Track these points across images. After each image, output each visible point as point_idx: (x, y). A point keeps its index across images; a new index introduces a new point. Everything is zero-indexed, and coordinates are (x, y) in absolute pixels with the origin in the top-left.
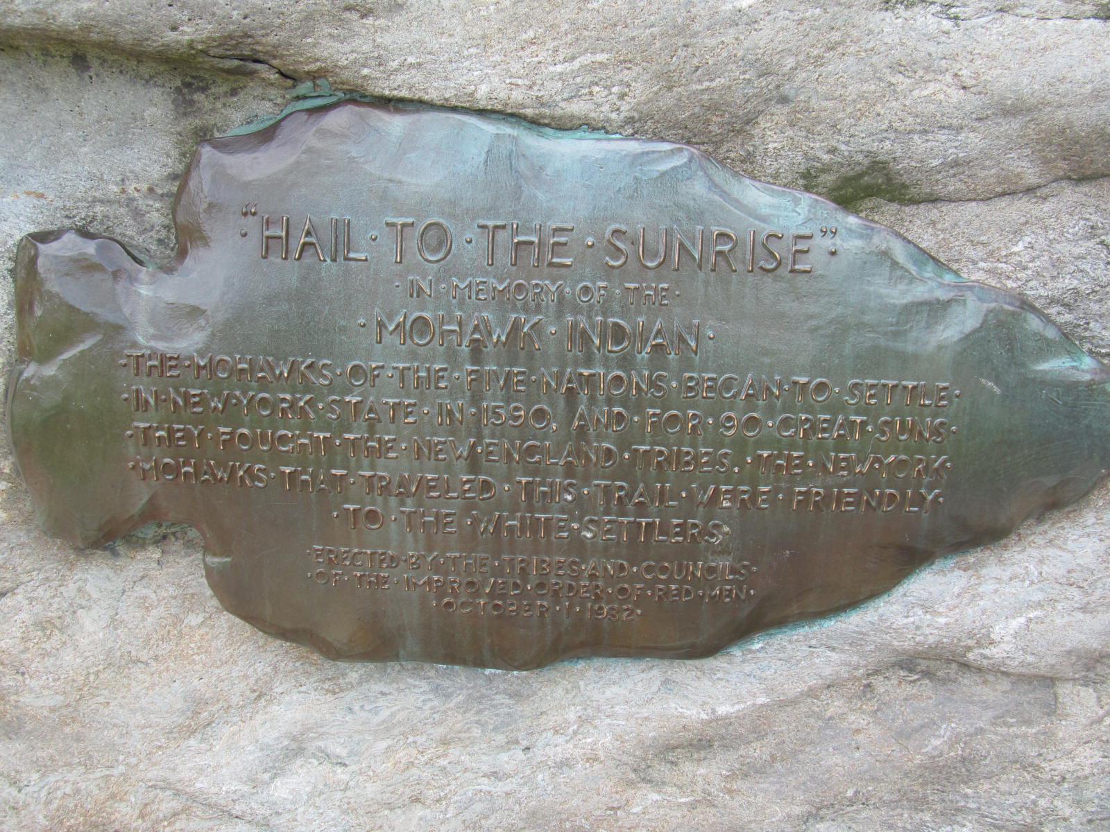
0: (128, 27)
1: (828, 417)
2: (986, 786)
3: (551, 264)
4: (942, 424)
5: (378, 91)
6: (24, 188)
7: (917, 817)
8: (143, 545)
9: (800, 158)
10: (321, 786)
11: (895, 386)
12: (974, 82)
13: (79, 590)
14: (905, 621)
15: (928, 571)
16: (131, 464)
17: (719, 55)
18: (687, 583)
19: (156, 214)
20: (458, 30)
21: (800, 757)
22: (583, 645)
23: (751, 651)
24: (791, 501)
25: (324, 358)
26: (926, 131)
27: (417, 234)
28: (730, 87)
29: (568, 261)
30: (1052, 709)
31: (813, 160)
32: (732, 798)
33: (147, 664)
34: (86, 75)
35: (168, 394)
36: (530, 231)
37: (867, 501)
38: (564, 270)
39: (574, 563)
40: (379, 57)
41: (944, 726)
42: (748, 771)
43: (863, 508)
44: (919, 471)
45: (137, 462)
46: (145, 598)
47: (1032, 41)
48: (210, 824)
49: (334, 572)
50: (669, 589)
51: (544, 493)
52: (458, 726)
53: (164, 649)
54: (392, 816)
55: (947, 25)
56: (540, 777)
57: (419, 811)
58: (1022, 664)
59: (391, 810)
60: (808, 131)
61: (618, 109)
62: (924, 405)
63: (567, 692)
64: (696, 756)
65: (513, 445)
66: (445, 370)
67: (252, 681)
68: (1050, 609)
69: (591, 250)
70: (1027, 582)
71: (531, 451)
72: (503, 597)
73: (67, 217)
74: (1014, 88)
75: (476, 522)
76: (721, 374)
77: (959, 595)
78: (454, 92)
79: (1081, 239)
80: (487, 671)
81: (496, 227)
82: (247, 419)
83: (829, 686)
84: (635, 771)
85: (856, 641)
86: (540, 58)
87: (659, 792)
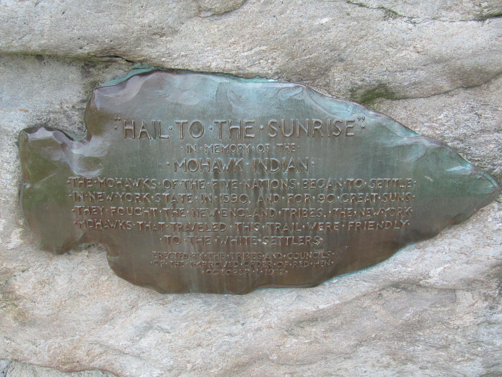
0: (61, 49)
1: (362, 194)
2: (428, 331)
3: (245, 137)
4: (409, 194)
5: (169, 67)
6: (19, 108)
7: (400, 344)
8: (80, 250)
9: (349, 84)
10: (160, 341)
11: (389, 181)
12: (422, 50)
13: (55, 268)
14: (395, 270)
15: (404, 250)
16: (75, 222)
17: (313, 44)
18: (306, 260)
19: (76, 117)
20: (202, 40)
21: (353, 323)
22: (264, 284)
23: (332, 283)
24: (347, 227)
25: (153, 178)
26: (402, 71)
27: (189, 127)
28: (318, 57)
29: (253, 136)
30: (454, 301)
31: (355, 84)
32: (326, 340)
33: (86, 296)
34: (42, 62)
35: (88, 194)
36: (236, 124)
37: (379, 226)
38: (251, 139)
39: (260, 254)
40: (169, 53)
41: (411, 309)
42: (333, 329)
43: (377, 228)
44: (400, 213)
45: (77, 221)
46: (83, 270)
47: (447, 32)
48: (116, 357)
49: (161, 261)
50: (299, 263)
51: (247, 228)
52: (215, 316)
53: (92, 290)
54: (189, 352)
55: (411, 26)
56: (249, 335)
57: (200, 350)
58: (442, 285)
59: (189, 350)
60: (352, 73)
61: (271, 69)
62: (401, 188)
63: (258, 301)
64: (311, 324)
65: (233, 210)
66: (204, 181)
67: (129, 301)
68: (453, 263)
69: (262, 131)
70: (444, 253)
71: (240, 212)
72: (231, 268)
73: (38, 119)
74: (439, 52)
75: (219, 240)
76: (318, 179)
77: (416, 259)
78: (201, 66)
79: (467, 113)
80: (226, 295)
81: (222, 123)
82: (122, 203)
83: (364, 296)
84: (287, 331)
85: (375, 278)
86: (238, 50)
87: (297, 339)
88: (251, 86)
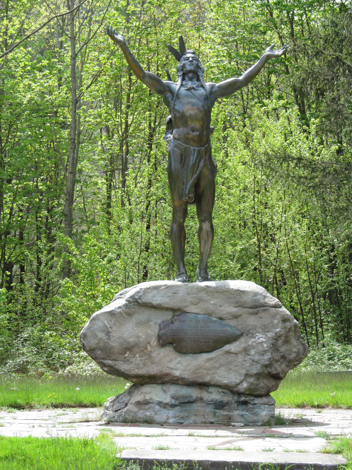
42: (215, 362)
88: (200, 316)
